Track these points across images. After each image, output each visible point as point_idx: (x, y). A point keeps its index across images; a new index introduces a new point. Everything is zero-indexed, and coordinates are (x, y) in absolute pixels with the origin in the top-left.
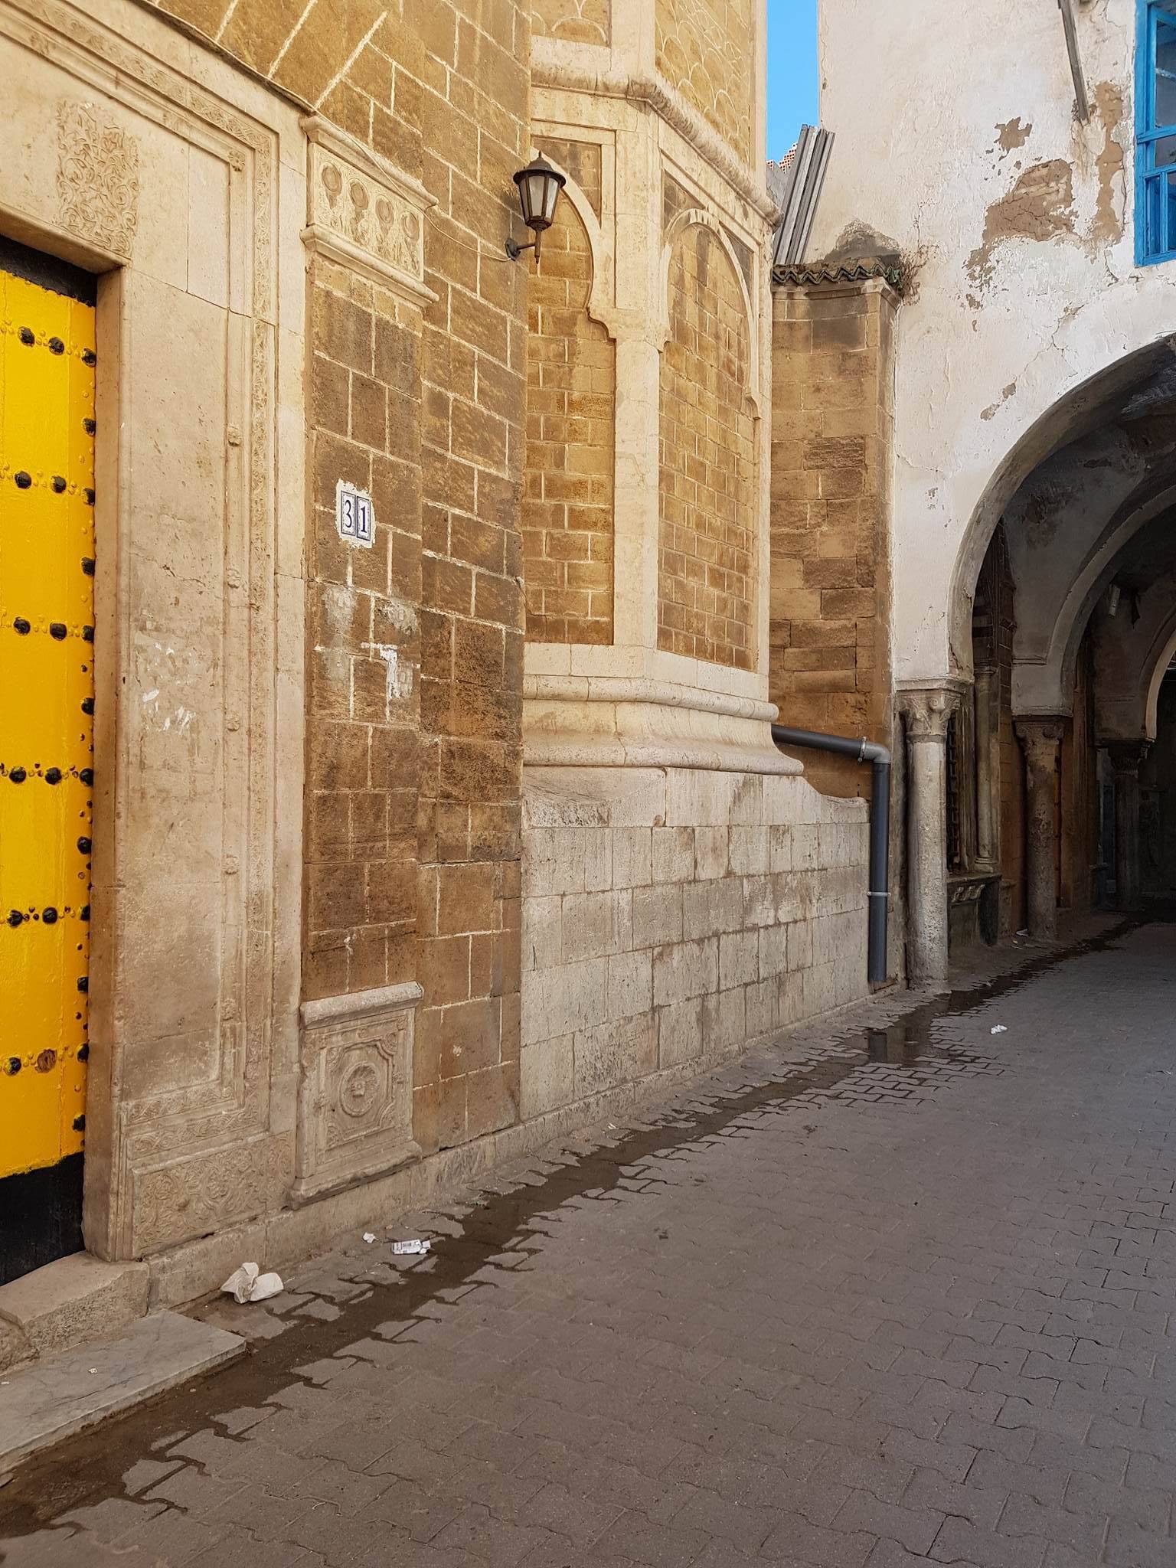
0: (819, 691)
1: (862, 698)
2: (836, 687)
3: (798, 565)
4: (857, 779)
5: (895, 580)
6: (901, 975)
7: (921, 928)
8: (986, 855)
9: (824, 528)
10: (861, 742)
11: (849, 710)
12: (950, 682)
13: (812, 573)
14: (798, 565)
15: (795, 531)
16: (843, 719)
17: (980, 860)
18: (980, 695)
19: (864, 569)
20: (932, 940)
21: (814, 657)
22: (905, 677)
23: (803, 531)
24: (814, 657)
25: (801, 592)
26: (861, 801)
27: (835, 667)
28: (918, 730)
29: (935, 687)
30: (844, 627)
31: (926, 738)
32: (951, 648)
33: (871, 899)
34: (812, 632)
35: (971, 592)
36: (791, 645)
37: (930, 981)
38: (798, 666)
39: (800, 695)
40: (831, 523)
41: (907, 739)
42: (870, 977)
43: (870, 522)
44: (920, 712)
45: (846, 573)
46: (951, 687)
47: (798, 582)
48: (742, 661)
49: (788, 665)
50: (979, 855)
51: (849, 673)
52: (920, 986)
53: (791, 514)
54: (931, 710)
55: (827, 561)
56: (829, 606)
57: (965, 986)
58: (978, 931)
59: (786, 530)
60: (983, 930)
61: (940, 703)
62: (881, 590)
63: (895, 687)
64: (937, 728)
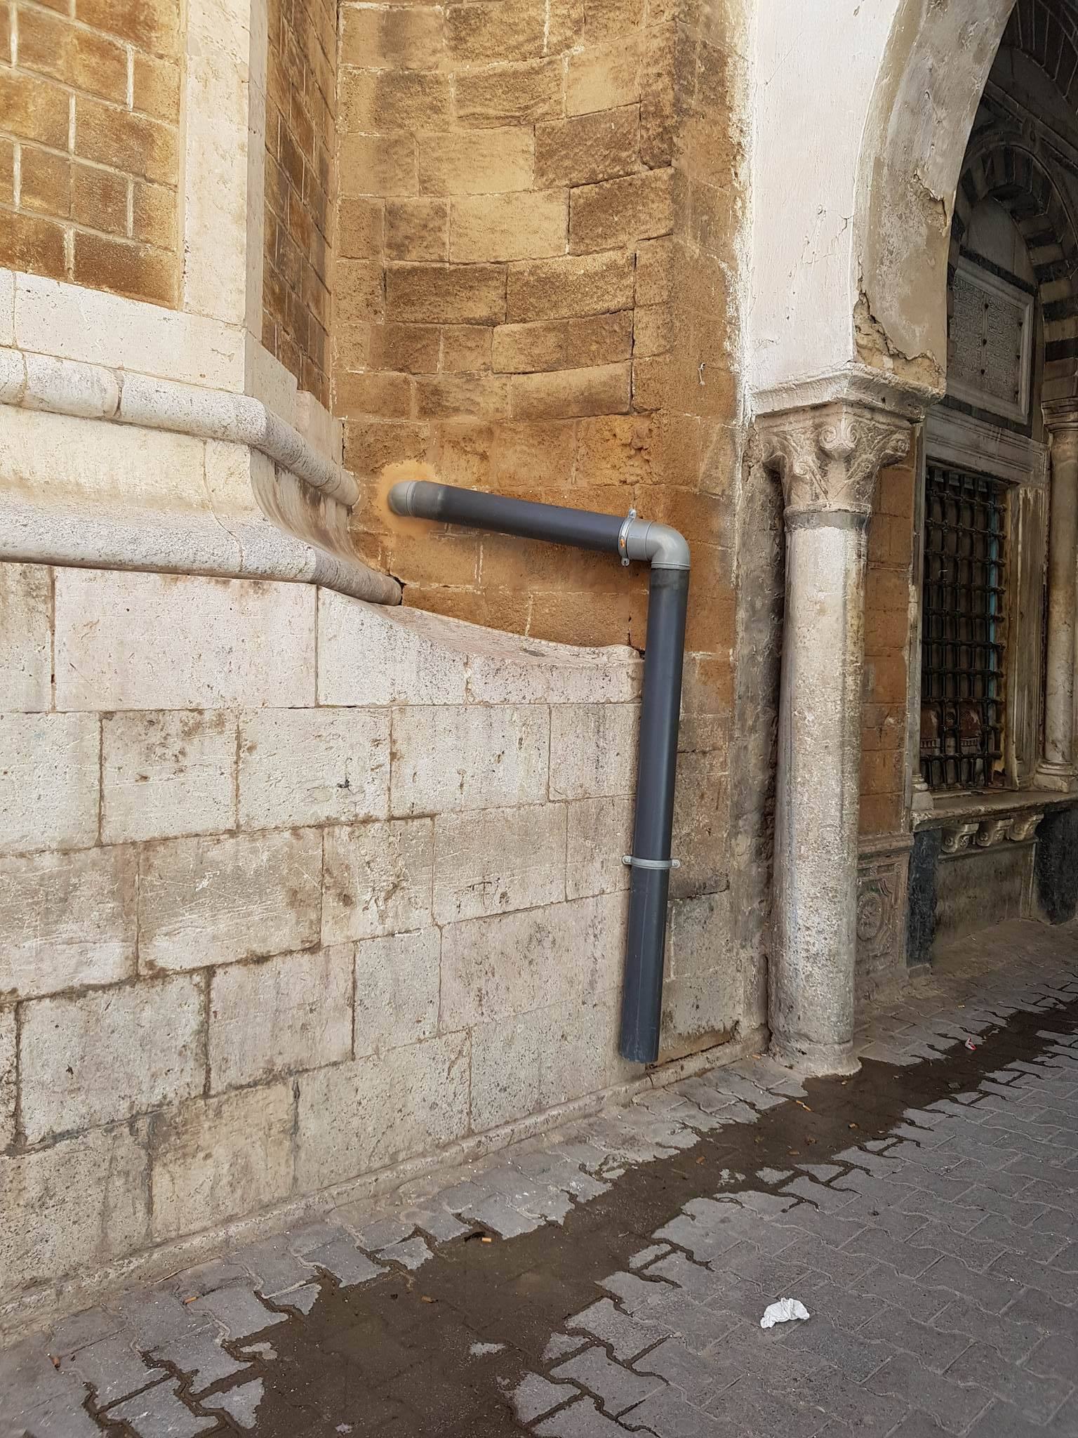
0: (560, 415)
1: (642, 425)
2: (595, 405)
3: (525, 140)
4: (622, 610)
5: (754, 171)
6: (749, 1024)
7: (789, 929)
8: (1058, 759)
9: (578, 49)
10: (620, 520)
11: (620, 454)
12: (864, 384)
13: (552, 153)
14: (525, 140)
15: (521, 66)
16: (607, 475)
17: (1046, 768)
18: (1059, 467)
19: (653, 126)
20: (813, 958)
21: (552, 340)
22: (769, 383)
23: (534, 62)
24: (552, 340)
25: (529, 200)
26: (622, 656)
27: (593, 360)
28: (800, 502)
29: (826, 398)
30: (612, 266)
31: (815, 516)
32: (865, 300)
33: (635, 876)
34: (550, 284)
35: (943, 180)
36: (508, 318)
37: (804, 1046)
38: (519, 362)
39: (521, 427)
40: (593, 37)
41: (781, 521)
42: (625, 1045)
43: (667, 15)
44: (802, 462)
45: (620, 142)
46: (868, 398)
47: (523, 177)
48: (125, 271)
49: (500, 361)
50: (1046, 761)
51: (619, 369)
52: (785, 1052)
53: (513, 28)
54: (824, 456)
55: (584, 121)
56: (586, 223)
57: (905, 1051)
58: (1033, 896)
59: (501, 65)
60: (1045, 893)
61: (840, 434)
62: (697, 174)
63: (750, 407)
64: (837, 492)
